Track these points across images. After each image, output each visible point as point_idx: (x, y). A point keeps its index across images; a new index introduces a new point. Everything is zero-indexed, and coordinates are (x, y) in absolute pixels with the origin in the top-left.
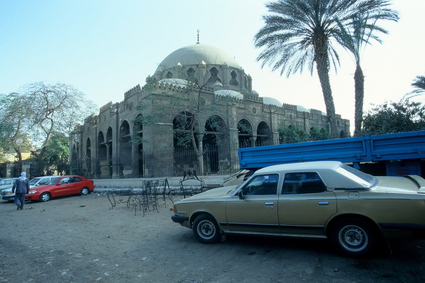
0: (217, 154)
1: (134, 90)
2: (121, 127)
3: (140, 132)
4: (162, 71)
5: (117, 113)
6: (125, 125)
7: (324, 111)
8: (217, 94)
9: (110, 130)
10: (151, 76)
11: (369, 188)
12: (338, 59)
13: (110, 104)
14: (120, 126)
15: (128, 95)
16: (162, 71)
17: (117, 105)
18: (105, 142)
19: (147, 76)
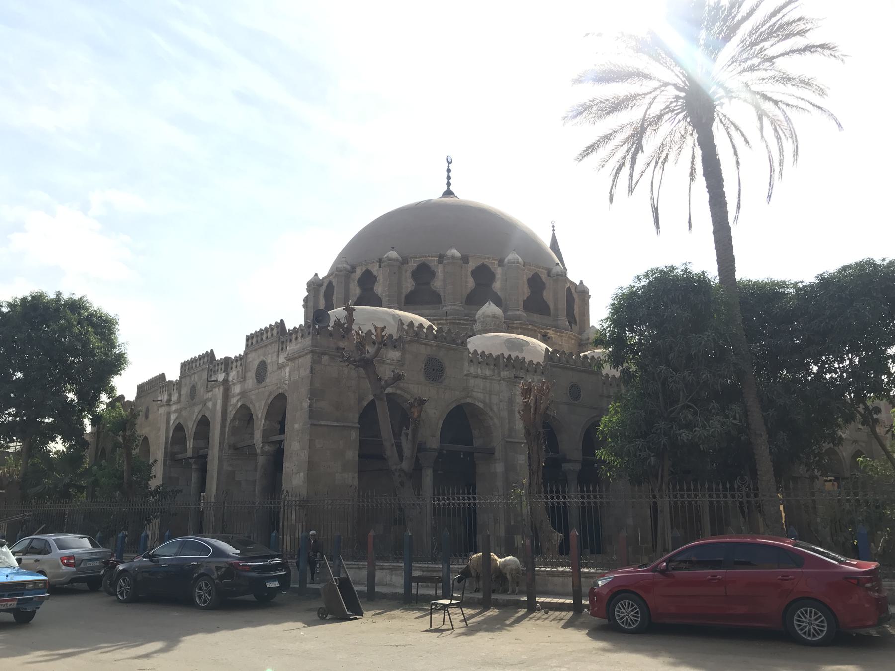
0: (475, 513)
1: (269, 334)
2: (233, 420)
3: (278, 438)
4: (348, 267)
5: (225, 381)
6: (246, 416)
7: (713, 273)
8: (476, 351)
9: (204, 423)
10: (321, 277)
11: (752, 104)
12: (738, 211)
13: (210, 355)
14: (230, 416)
15: (255, 340)
16: (348, 267)
17: (227, 362)
18: (190, 453)
19: (310, 277)
